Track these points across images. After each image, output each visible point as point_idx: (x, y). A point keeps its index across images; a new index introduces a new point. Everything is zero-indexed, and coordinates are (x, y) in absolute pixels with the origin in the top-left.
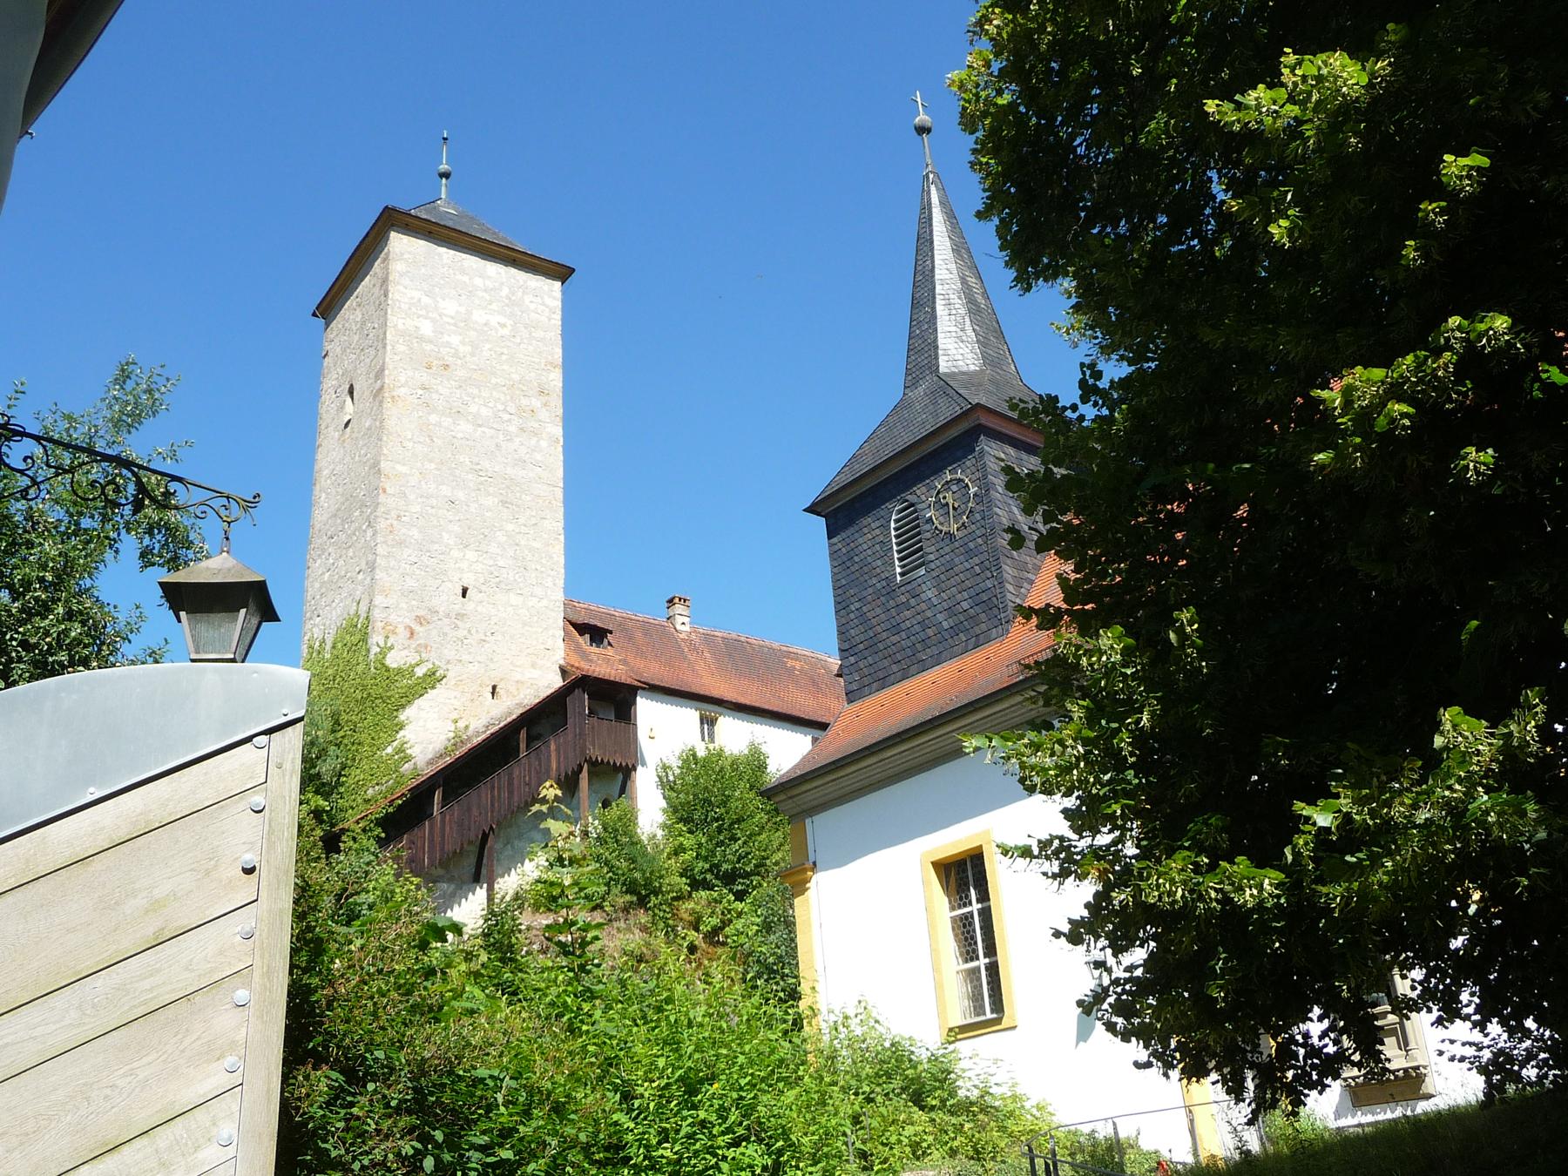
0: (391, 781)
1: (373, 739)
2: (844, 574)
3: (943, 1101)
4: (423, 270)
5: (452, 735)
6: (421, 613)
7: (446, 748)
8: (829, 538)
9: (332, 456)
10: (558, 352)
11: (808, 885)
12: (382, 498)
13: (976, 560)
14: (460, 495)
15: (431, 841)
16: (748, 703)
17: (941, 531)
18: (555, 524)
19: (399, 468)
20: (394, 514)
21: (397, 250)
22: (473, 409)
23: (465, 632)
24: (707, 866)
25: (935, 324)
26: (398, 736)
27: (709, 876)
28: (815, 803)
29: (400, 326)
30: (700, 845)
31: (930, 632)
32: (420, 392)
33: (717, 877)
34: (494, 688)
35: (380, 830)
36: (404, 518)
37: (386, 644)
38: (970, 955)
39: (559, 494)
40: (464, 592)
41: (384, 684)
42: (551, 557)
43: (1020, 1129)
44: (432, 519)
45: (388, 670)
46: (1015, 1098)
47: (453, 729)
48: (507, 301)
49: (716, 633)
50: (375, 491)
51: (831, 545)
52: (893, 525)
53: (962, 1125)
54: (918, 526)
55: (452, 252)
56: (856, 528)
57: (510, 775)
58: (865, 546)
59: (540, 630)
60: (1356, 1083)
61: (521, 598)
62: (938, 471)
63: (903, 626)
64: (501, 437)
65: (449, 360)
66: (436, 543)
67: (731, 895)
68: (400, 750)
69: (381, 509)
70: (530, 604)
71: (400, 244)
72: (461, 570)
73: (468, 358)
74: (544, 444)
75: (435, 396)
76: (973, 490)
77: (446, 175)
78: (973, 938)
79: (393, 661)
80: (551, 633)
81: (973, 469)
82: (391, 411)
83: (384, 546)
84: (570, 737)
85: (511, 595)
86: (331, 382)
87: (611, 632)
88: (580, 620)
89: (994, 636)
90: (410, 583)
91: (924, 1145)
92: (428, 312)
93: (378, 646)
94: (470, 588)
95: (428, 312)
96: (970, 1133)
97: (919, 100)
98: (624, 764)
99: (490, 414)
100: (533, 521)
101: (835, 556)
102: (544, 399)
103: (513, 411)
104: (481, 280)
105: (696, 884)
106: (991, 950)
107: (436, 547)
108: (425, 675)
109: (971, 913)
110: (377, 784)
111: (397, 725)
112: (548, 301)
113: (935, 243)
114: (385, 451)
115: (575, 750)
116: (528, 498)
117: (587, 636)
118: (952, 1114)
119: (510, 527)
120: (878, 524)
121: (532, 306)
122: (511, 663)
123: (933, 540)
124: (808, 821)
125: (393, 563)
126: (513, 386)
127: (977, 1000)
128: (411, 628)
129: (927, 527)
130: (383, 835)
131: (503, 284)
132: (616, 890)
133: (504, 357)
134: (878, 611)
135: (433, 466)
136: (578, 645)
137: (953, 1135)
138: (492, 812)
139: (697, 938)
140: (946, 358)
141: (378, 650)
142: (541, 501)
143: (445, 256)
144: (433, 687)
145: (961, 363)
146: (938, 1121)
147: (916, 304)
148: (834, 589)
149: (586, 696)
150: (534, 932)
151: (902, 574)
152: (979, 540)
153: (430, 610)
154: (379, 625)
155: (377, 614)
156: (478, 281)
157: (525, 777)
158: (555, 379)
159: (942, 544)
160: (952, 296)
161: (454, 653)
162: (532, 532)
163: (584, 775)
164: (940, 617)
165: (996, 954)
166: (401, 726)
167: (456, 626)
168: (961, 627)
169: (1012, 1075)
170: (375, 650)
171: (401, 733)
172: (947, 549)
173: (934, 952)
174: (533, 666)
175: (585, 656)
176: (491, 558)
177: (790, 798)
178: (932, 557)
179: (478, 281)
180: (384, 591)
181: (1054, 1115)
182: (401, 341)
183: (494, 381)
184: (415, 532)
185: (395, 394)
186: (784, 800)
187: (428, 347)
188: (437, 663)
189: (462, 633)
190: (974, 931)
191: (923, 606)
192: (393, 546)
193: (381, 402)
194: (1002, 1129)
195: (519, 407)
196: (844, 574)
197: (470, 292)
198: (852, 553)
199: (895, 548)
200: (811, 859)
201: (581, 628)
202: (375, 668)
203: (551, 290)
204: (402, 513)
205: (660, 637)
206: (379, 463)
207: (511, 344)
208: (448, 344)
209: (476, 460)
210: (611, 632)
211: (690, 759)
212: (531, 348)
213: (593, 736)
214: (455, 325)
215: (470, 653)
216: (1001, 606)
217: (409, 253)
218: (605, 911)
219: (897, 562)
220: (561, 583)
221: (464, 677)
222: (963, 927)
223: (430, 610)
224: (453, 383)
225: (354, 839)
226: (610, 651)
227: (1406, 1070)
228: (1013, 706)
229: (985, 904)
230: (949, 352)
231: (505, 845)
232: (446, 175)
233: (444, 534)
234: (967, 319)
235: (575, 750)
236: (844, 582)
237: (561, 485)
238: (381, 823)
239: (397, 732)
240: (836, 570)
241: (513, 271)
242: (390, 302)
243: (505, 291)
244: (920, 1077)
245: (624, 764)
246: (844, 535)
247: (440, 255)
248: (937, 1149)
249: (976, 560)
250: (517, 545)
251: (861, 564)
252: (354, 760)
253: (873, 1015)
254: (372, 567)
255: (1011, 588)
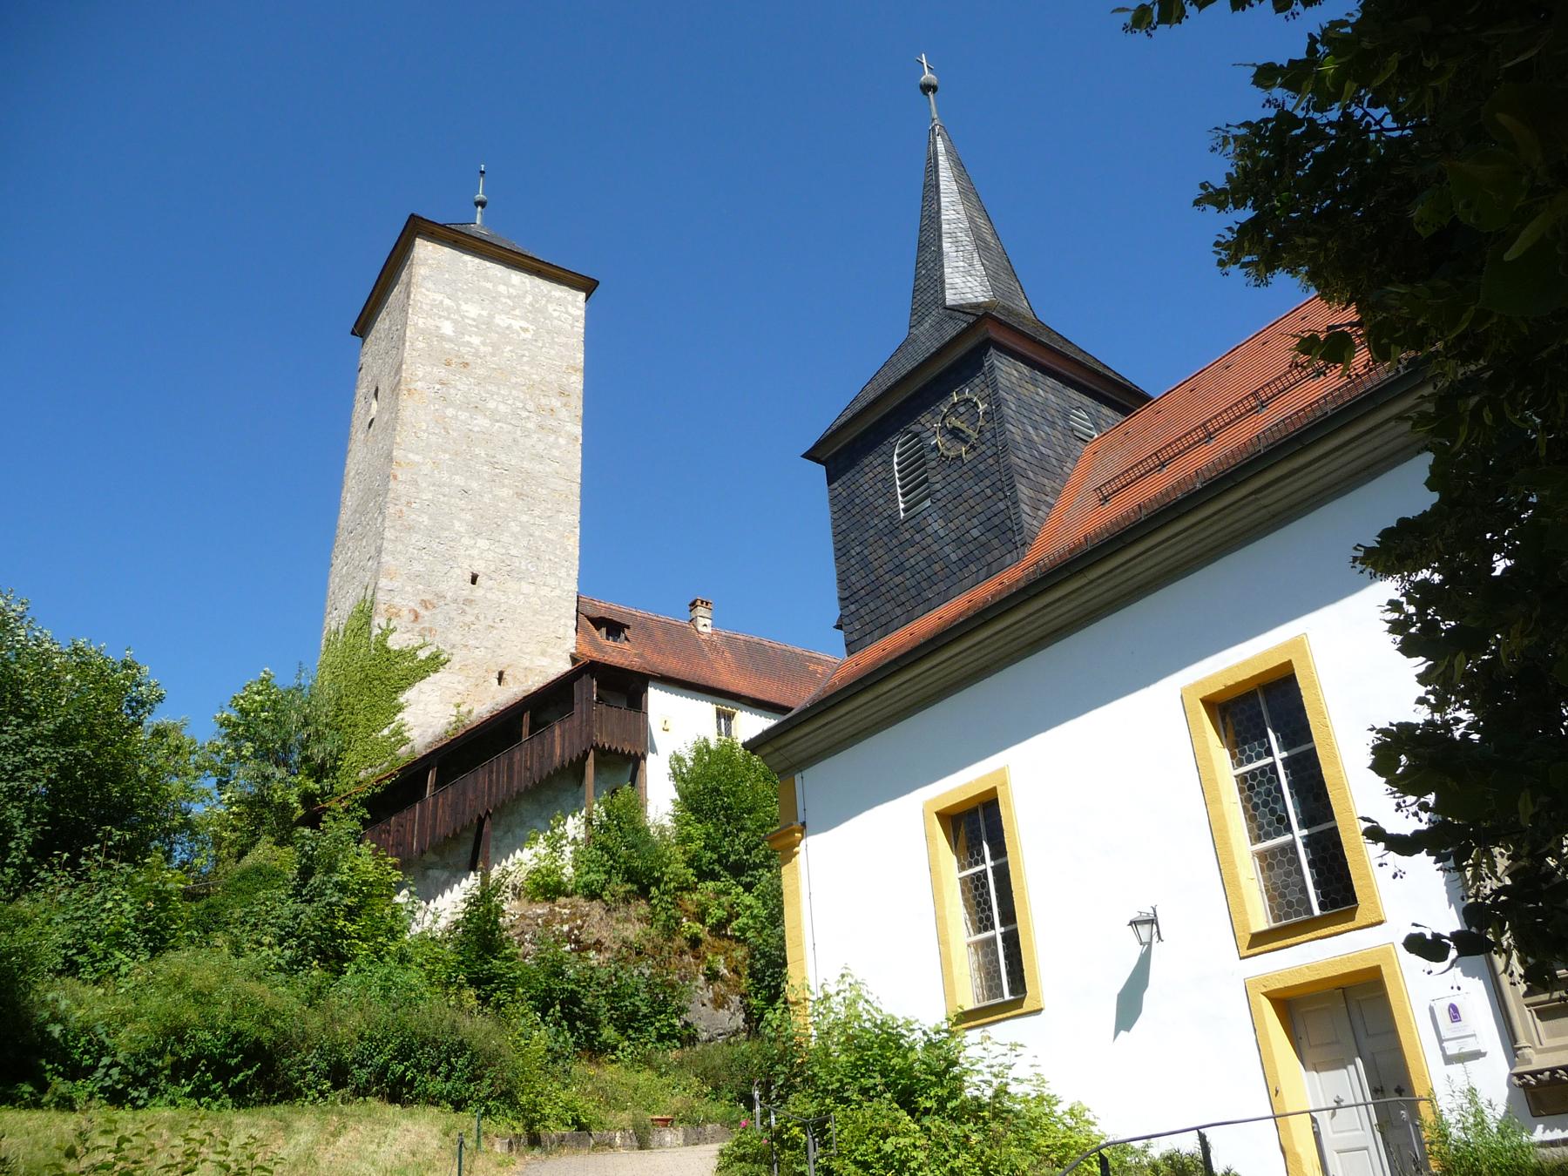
0: (386, 764)
1: (368, 720)
2: (845, 518)
3: (942, 1102)
4: (447, 276)
5: (454, 719)
6: (427, 597)
7: (447, 732)
8: (829, 484)
9: (359, 456)
10: (580, 357)
11: (796, 849)
12: (392, 484)
13: (987, 482)
14: (475, 485)
15: (422, 825)
16: (766, 699)
17: (947, 458)
18: (570, 517)
19: (411, 456)
20: (404, 500)
21: (421, 256)
22: (491, 405)
23: (473, 618)
24: (715, 857)
25: (941, 260)
26: (397, 718)
27: (717, 867)
28: (804, 755)
29: (421, 324)
30: (708, 835)
31: (937, 567)
32: (438, 386)
33: (726, 868)
34: (501, 674)
35: (365, 811)
36: (414, 505)
37: (388, 625)
38: (984, 923)
39: (577, 489)
40: (474, 580)
41: (383, 665)
42: (566, 549)
43: (1049, 1143)
44: (444, 506)
45: (388, 651)
46: (1041, 1099)
47: (455, 713)
48: (530, 308)
49: (739, 637)
50: (387, 477)
51: (831, 491)
52: (896, 459)
53: (967, 1137)
54: (923, 456)
55: (477, 260)
56: (857, 468)
57: (511, 759)
58: (866, 486)
59: (552, 619)
60: (1539, 1081)
61: (533, 587)
62: (946, 394)
63: (907, 565)
64: (519, 432)
65: (469, 358)
66: (448, 530)
67: (740, 887)
68: (398, 732)
69: (391, 495)
70: (542, 593)
71: (425, 252)
72: (472, 558)
73: (488, 358)
74: (562, 441)
75: (452, 391)
76: (982, 407)
77: (482, 204)
78: (987, 902)
79: (394, 642)
80: (562, 622)
81: (982, 386)
82: (408, 406)
83: (392, 530)
84: (576, 722)
85: (523, 583)
86: (363, 389)
87: (628, 627)
88: (596, 615)
89: (1008, 562)
90: (417, 567)
91: (913, 1165)
92: (449, 314)
93: (380, 628)
94: (481, 575)
95: (449, 314)
96: (978, 1150)
97: (924, 61)
98: (633, 752)
99: (509, 411)
100: (549, 514)
101: (836, 501)
102: (564, 400)
103: (532, 410)
104: (505, 288)
105: (703, 875)
106: (1009, 916)
107: (447, 533)
108: (428, 658)
109: (984, 872)
110: (371, 766)
111: (395, 707)
112: (571, 310)
113: (941, 187)
114: (398, 440)
115: (581, 736)
116: (544, 492)
117: (604, 630)
118: (955, 1119)
119: (524, 518)
120: (879, 460)
121: (556, 314)
122: (520, 650)
123: (939, 469)
124: (797, 777)
125: (400, 547)
126: (533, 386)
127: (992, 979)
128: (415, 611)
129: (933, 455)
130: (368, 816)
131: (526, 292)
132: (617, 879)
133: (525, 359)
134: (880, 552)
135: (447, 456)
136: (594, 639)
137: (954, 1151)
138: (490, 795)
139: (702, 930)
140: (953, 291)
141: (380, 631)
142: (557, 495)
143: (470, 264)
144: (436, 671)
145: (970, 296)
146: (934, 1130)
147: (922, 247)
148: (834, 543)
149: (595, 683)
150: (528, 921)
151: (905, 510)
152: (991, 461)
153: (436, 594)
154: (382, 607)
155: (380, 596)
156: (502, 289)
157: (526, 761)
158: (576, 382)
159: (949, 471)
160: (959, 234)
161: (459, 637)
162: (547, 524)
163: (591, 761)
164: (947, 549)
165: (1014, 921)
166: (400, 708)
167: (464, 612)
168: (971, 557)
169: (1038, 1070)
170: (376, 631)
171: (400, 716)
172: (955, 476)
173: (940, 921)
174: (543, 653)
175: (599, 648)
176: (503, 547)
177: (777, 750)
178: (938, 486)
179: (502, 289)
180: (390, 574)
181: (1093, 1124)
182: (420, 338)
183: (514, 380)
184: (425, 519)
185: (411, 387)
186: (771, 753)
187: (447, 346)
188: (441, 647)
189: (469, 618)
190: (988, 893)
191: (929, 540)
192: (401, 531)
193: (398, 394)
194: (1024, 1142)
195: (539, 406)
196: (845, 518)
197: (493, 297)
198: (853, 496)
199: (898, 483)
200: (801, 819)
201: (598, 622)
202: (375, 649)
203: (575, 301)
204: (412, 500)
205: (684, 637)
206: (391, 453)
207: (533, 348)
208: (469, 344)
209: (492, 452)
210: (628, 627)
211: (702, 750)
212: (553, 352)
213: (601, 722)
214: (476, 327)
215: (477, 639)
216: (1015, 528)
217: (434, 259)
218: (604, 901)
219: (900, 498)
220: (575, 574)
221: (470, 661)
222: (975, 889)
223: (436, 594)
224: (472, 380)
225: (335, 819)
226: (627, 646)
227: (1553, 1071)
228: (1031, 615)
229: (1010, 927)
230: (957, 286)
231: (506, 833)
232: (482, 204)
233: (455, 521)
234: (976, 255)
235: (581, 736)
236: (844, 527)
237: (579, 481)
238: (364, 803)
239: (395, 715)
240: (836, 516)
241: (538, 281)
242: (411, 302)
243: (529, 299)
244: (911, 1068)
245: (633, 752)
246: (844, 478)
247: (465, 263)
248: (932, 1172)
249: (987, 482)
250: (531, 535)
251: (862, 506)
252: (350, 742)
253: (864, 993)
254: (379, 551)
255: (1027, 509)
